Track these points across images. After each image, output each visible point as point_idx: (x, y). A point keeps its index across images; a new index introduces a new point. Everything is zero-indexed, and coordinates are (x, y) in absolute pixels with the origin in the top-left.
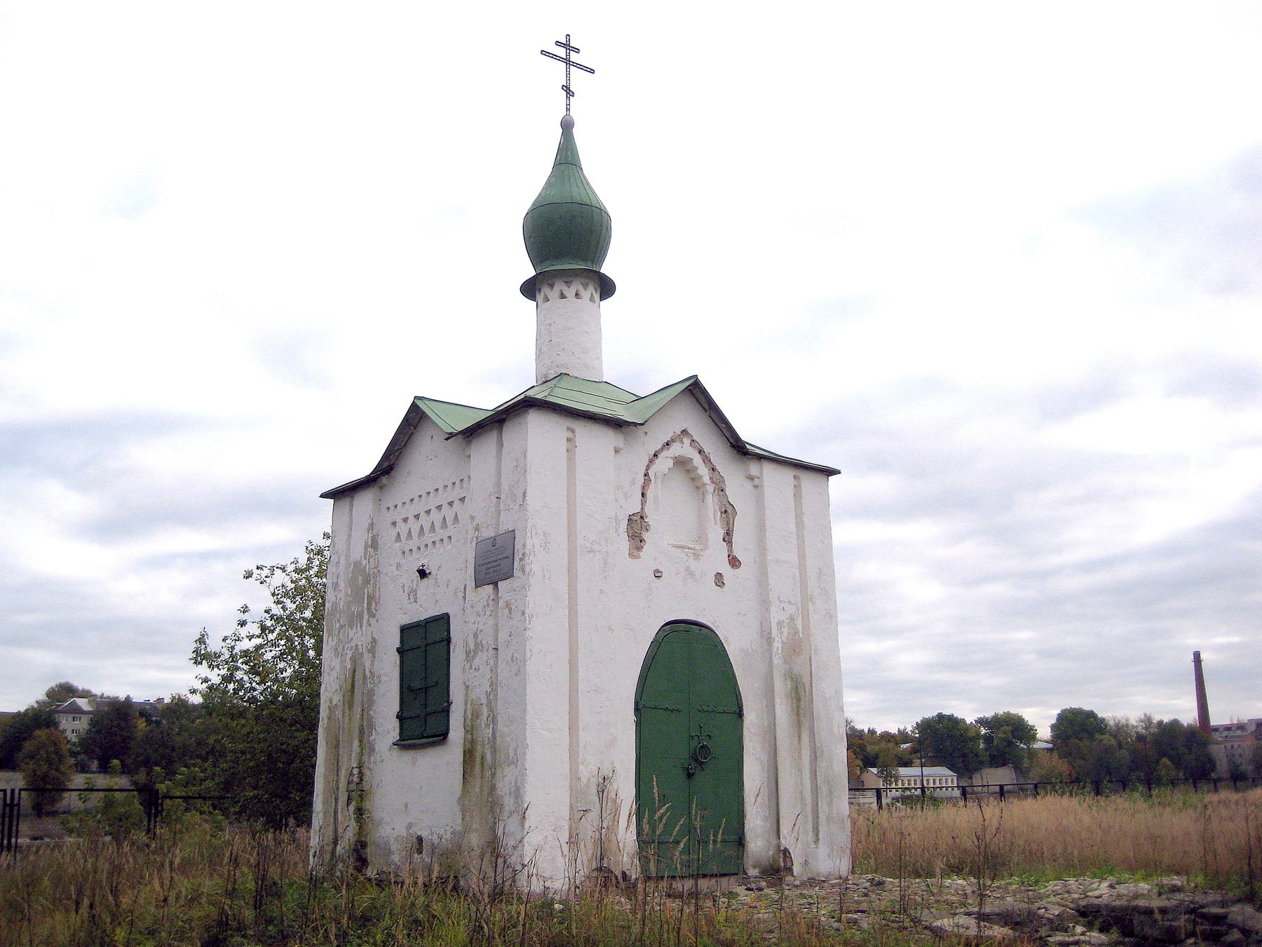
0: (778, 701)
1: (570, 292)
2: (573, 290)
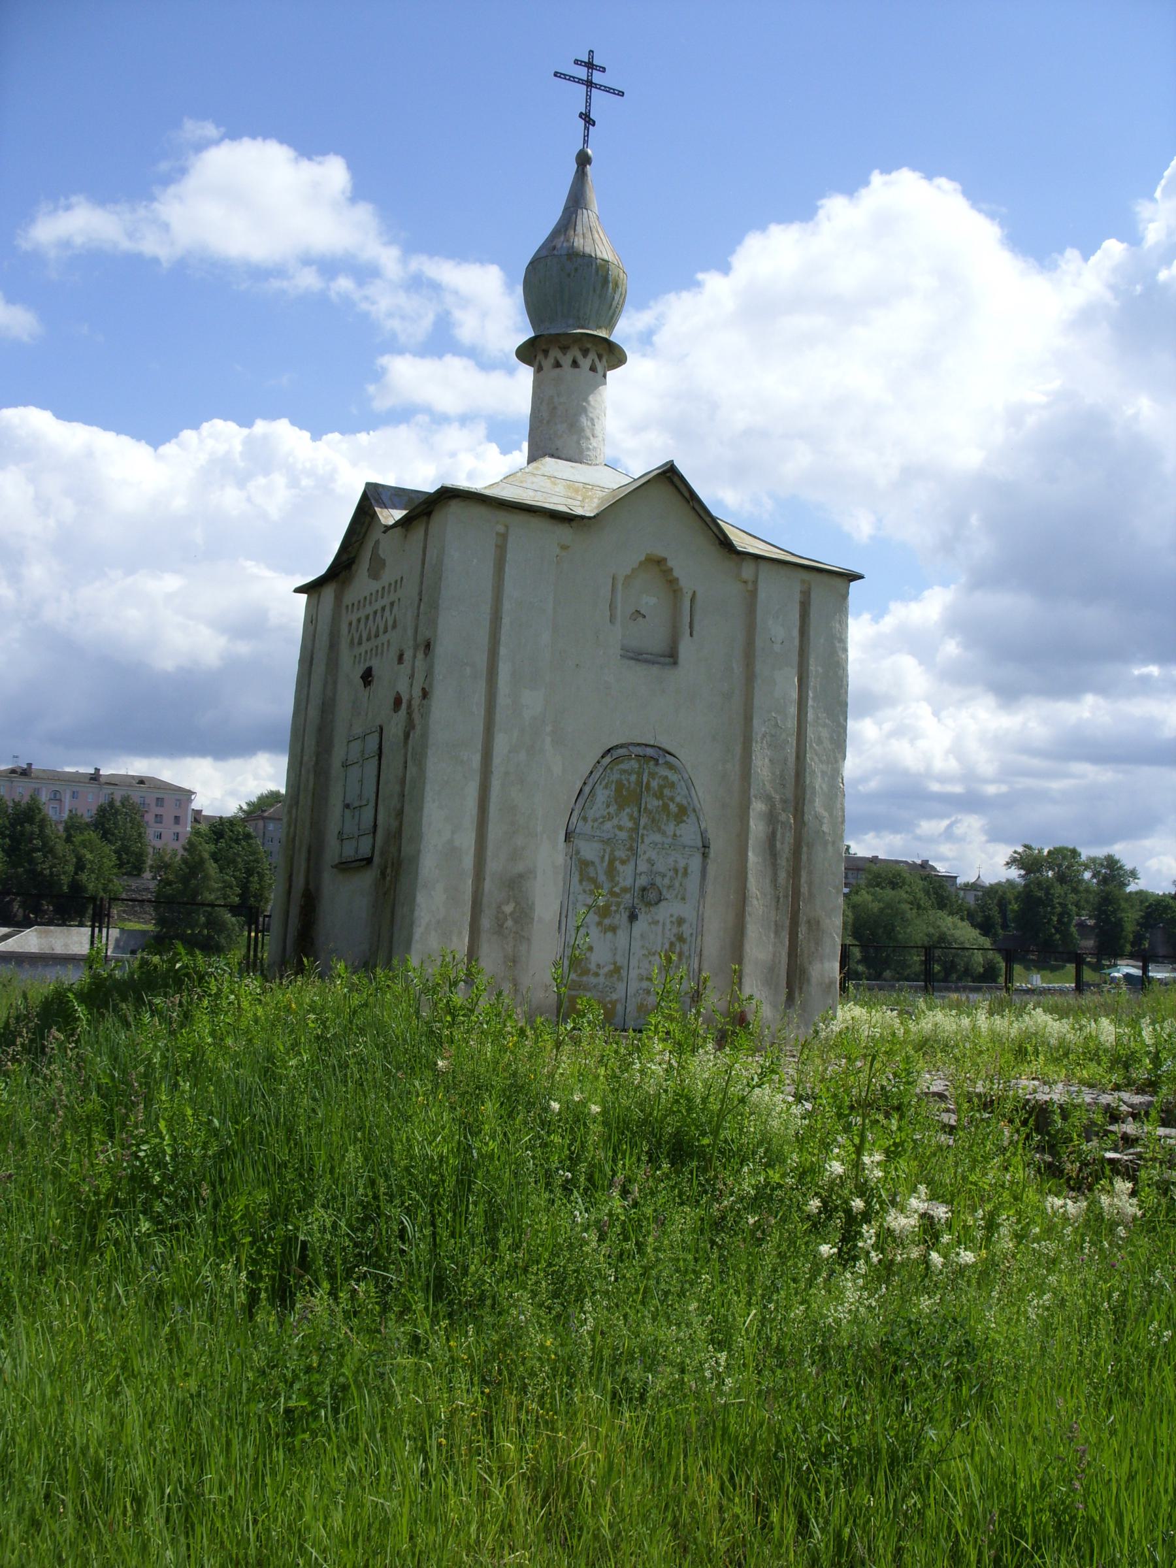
0: (752, 856)
1: (566, 360)
2: (550, 361)
